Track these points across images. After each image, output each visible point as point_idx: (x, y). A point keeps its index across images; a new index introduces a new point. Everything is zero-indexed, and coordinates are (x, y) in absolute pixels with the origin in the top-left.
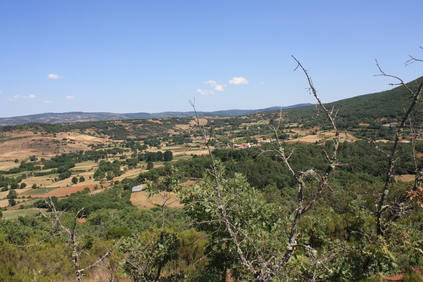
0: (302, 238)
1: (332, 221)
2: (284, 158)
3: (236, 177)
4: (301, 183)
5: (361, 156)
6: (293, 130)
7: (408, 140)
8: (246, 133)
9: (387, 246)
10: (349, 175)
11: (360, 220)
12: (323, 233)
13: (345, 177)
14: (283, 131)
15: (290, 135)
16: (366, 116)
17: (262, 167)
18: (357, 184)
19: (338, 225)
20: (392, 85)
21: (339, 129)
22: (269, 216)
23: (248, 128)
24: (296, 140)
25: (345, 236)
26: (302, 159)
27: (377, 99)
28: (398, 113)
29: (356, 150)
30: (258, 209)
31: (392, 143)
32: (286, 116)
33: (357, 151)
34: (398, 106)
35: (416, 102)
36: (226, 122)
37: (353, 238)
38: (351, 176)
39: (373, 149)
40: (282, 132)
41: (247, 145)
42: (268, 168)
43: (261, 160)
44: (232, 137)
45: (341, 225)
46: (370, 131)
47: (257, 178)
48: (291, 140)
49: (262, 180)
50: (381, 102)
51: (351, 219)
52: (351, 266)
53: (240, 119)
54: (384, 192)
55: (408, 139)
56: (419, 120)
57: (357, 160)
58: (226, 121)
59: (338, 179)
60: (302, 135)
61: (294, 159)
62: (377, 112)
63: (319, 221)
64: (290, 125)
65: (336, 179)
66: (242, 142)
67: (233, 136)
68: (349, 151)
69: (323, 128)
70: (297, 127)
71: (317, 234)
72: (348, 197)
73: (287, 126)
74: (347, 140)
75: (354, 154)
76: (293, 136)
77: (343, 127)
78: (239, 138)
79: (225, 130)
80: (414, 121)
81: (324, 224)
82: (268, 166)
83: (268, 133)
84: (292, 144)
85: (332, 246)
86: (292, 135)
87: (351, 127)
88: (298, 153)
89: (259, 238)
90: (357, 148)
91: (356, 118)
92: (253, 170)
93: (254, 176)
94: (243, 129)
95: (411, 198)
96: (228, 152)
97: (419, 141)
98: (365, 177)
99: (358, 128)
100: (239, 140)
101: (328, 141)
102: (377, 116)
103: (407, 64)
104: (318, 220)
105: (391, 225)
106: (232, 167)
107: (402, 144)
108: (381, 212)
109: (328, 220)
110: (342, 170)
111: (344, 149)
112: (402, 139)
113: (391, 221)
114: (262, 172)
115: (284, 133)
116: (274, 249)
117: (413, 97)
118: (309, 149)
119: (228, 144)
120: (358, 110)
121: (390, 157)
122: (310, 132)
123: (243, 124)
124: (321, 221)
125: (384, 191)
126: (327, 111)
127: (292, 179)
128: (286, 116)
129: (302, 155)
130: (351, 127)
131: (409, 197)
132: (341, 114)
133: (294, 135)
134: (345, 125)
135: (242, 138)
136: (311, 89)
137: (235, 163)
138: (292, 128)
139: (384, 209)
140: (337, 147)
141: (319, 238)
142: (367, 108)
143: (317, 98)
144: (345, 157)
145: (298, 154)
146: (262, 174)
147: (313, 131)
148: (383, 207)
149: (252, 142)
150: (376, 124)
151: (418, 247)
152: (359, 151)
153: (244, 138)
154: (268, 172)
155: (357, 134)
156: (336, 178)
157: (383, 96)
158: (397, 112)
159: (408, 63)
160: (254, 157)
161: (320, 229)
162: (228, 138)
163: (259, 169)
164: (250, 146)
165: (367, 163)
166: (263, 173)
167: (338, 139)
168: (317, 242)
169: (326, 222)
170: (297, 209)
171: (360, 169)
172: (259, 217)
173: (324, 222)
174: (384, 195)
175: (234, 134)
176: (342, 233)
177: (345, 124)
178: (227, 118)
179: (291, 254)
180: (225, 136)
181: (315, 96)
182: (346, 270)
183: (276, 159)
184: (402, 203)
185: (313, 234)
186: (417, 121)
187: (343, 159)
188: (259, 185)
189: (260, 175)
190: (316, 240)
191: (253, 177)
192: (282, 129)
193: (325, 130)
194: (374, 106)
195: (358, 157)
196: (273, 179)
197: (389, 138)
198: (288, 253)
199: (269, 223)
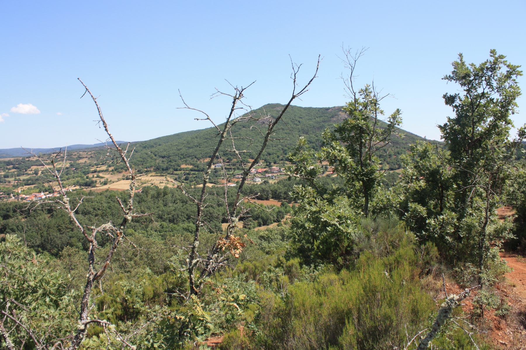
0: (104, 311)
1: (149, 285)
2: (70, 211)
3: (7, 240)
4: (92, 242)
5: (184, 204)
6: (101, 175)
7: (235, 184)
8: (37, 180)
9: (202, 305)
10: (171, 226)
11: (182, 279)
12: (139, 300)
13: (167, 230)
14: (88, 176)
15: (98, 181)
16: (189, 157)
17: (62, 224)
18: (178, 237)
19: (157, 288)
20: (198, 120)
21: (158, 172)
22: (54, 288)
23: (40, 173)
24: (106, 187)
25: (166, 301)
26: (114, 211)
27: (200, 137)
29: (178, 197)
30: (37, 281)
31: (217, 187)
32: (91, 157)
33: (179, 197)
35: (223, 139)
36: (8, 165)
37: (174, 302)
38: (174, 228)
39: (198, 194)
40: (87, 178)
41: (40, 196)
42: (70, 224)
43: (60, 215)
44: (18, 185)
45: (161, 287)
46: (194, 174)
47: (55, 239)
48: (99, 187)
49: (62, 241)
50: (204, 141)
51: (172, 279)
52: (164, 335)
53: (29, 160)
54: (195, 244)
56: (244, 161)
57: (180, 208)
58: (8, 163)
59: (159, 233)
60: (113, 180)
61: (104, 211)
62: (200, 152)
63: (133, 286)
64: (97, 168)
65: (156, 233)
66: (32, 191)
67: (19, 184)
68: (170, 198)
69: (138, 171)
70: (107, 171)
71: (132, 303)
72: (168, 253)
73: (94, 169)
74: (168, 185)
75: (176, 202)
76: (102, 182)
77: (163, 170)
78: (27, 187)
79: (6, 176)
81: (139, 290)
82: (70, 222)
83: (68, 179)
84: (101, 191)
85: (151, 315)
86: (100, 181)
87: (171, 170)
88: (109, 203)
89: (45, 320)
90: (179, 194)
91: (177, 158)
92: (49, 228)
93: (52, 237)
94: (33, 174)
95: (224, 248)
96: (11, 206)
98: (190, 228)
99: (180, 170)
100: (28, 189)
101: (145, 187)
102: (200, 156)
103: (212, 97)
104: (132, 285)
105: (205, 281)
106: (18, 226)
108: (193, 267)
109: (145, 283)
110: (163, 221)
111: (164, 196)
113: (205, 277)
114: (62, 231)
115: (90, 179)
116: (66, 331)
117: (220, 135)
118: (122, 198)
119: (12, 195)
120: (179, 150)
121: (198, 203)
122: (123, 176)
123: (34, 168)
124: (135, 286)
125: (194, 243)
126: (120, 150)
127: (102, 236)
128: (91, 157)
129: (114, 206)
130: (171, 170)
131: (221, 248)
132: (160, 154)
133: (103, 180)
134: (165, 167)
135: (33, 186)
136: (102, 122)
137: (23, 220)
138: (99, 172)
139: (196, 264)
140: (133, 194)
141: (135, 307)
142: (189, 148)
143: (108, 133)
144: (166, 206)
145: (109, 205)
146: (62, 232)
147: (126, 175)
148: (194, 261)
149: (46, 191)
150: (200, 165)
151: (233, 301)
152: (181, 197)
153: (34, 187)
154: (70, 230)
155: (179, 178)
156: (156, 231)
157: (207, 134)
159: (214, 96)
160: (50, 211)
161: (135, 296)
162: (11, 186)
163: (57, 227)
164: (44, 197)
165: (192, 211)
166: (63, 231)
167: (134, 184)
168: (133, 313)
169: (142, 287)
170: (88, 275)
171: (184, 219)
172: (40, 291)
173: (139, 287)
174: (194, 247)
175: (21, 181)
176: (162, 297)
177: (165, 166)
178: (9, 159)
179: (83, 335)
180: (7, 184)
181: (106, 130)
182: (158, 342)
183: (81, 212)
184: (215, 255)
185: (126, 304)
187: (164, 208)
188: (58, 248)
189: (59, 235)
190: (131, 310)
191: (49, 238)
192: (86, 173)
193: (141, 173)
194: (198, 145)
195: (181, 204)
196: (78, 238)
197: (215, 181)
198: (79, 334)
199: (54, 298)
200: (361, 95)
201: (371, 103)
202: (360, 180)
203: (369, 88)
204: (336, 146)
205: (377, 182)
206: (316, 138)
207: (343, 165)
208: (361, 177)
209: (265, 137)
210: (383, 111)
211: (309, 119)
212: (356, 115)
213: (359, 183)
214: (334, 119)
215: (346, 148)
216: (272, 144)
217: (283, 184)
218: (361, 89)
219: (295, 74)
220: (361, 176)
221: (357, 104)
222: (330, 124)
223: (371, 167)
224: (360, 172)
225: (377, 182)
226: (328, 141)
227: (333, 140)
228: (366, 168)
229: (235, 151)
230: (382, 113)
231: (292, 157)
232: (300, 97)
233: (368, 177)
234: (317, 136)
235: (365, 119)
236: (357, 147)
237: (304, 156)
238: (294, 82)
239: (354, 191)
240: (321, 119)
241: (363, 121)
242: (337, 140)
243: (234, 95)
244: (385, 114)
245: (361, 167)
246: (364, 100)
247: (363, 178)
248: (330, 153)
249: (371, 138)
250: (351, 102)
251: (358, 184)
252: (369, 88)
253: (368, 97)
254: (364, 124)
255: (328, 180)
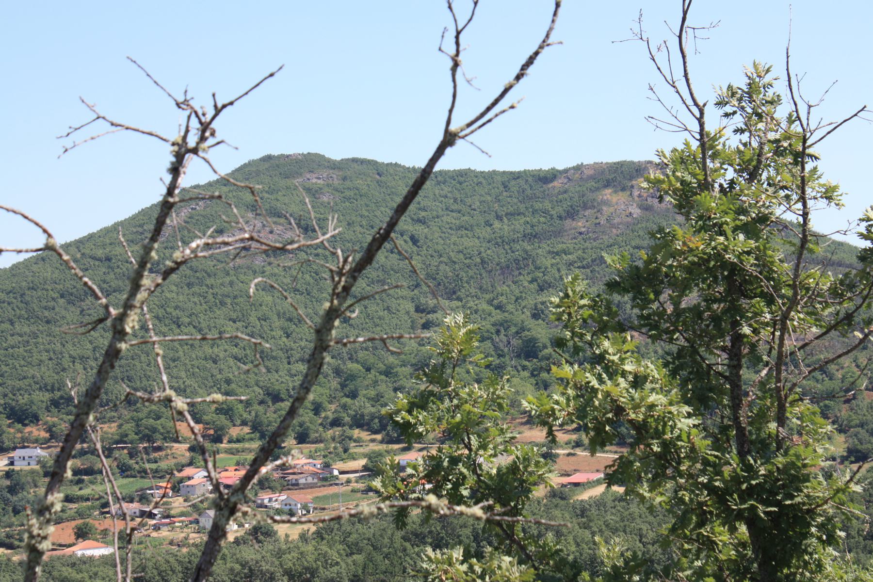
28: (47, 396)
34: (45, 356)
35: (123, 346)
55: (105, 532)
56: (154, 430)
80: (132, 436)
97: (159, 543)
103: (68, 142)
107: (73, 565)
112: (73, 538)
117: (109, 322)
158: (44, 388)
159: (76, 136)
186: (149, 438)
200: (727, 115)
201: (779, 152)
202: (739, 516)
203: (767, 79)
204: (622, 360)
205: (821, 527)
206: (498, 316)
207: (656, 449)
208: (743, 501)
209: (318, 331)
210: (834, 189)
211: (459, 228)
212: (708, 210)
213: (733, 530)
214: (580, 224)
215: (666, 365)
216: (287, 350)
217: (343, 542)
218: (730, 87)
219: (458, 33)
220: (744, 496)
221: (714, 157)
222: (560, 247)
223: (786, 454)
224: (736, 479)
225: (821, 527)
226: (581, 336)
227: (603, 329)
228: (767, 461)
229: (169, 400)
230: (829, 198)
231: (410, 412)
232: (479, 137)
233: (778, 504)
234: (499, 307)
235: (750, 230)
236: (719, 361)
237: (467, 407)
238: (456, 65)
239: (710, 569)
240: (519, 224)
241: (741, 237)
242: (621, 328)
243: (176, 136)
244: (844, 200)
245: (742, 454)
246: (745, 137)
247: (753, 508)
248: (594, 391)
249: (785, 317)
250: (680, 147)
251: (726, 537)
252: (767, 79)
253: (761, 126)
254: (748, 253)
255: (557, 513)
